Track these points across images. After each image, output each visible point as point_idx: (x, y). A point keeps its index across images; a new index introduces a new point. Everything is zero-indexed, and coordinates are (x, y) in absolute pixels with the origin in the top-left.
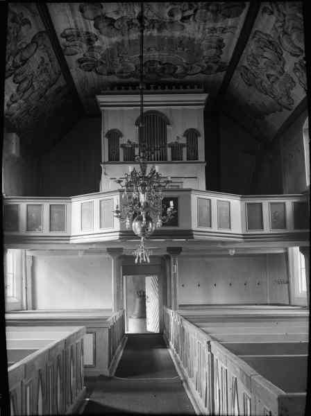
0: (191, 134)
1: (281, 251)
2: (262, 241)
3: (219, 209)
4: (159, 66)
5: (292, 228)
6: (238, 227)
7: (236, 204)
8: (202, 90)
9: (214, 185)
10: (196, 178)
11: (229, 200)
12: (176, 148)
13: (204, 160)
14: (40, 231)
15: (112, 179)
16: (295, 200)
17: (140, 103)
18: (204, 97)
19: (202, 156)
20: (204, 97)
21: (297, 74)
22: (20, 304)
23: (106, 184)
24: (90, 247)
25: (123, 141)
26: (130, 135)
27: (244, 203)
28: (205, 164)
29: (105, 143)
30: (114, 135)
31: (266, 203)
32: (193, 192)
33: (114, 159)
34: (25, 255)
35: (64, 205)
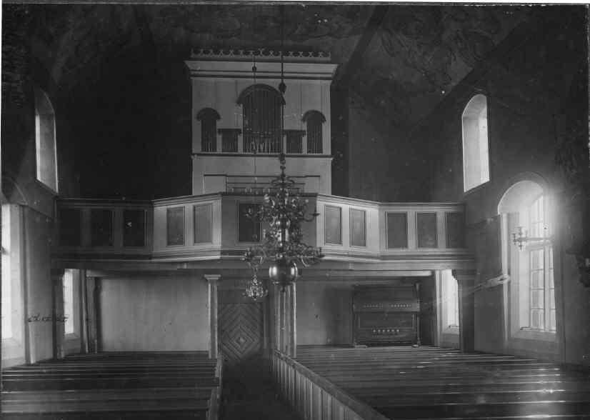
0: (314, 119)
1: (428, 274)
2: (530, 264)
3: (352, 221)
4: (22, 51)
5: (384, 244)
6: (376, 242)
7: (373, 212)
8: (329, 59)
9: (340, 189)
10: (319, 176)
11: (340, 205)
12: (294, 136)
13: (330, 153)
14: (111, 245)
15: (205, 175)
16: (451, 210)
17: (280, 75)
18: (331, 68)
19: (327, 150)
20: (331, 68)
21: (459, 44)
22: (79, 342)
23: (201, 185)
24: (179, 267)
25: (220, 124)
26: (233, 117)
27: (383, 214)
28: (332, 159)
29: (197, 126)
30: (210, 116)
31: (412, 212)
32: (318, 197)
33: (208, 147)
34: (86, 277)
35: (182, 208)
